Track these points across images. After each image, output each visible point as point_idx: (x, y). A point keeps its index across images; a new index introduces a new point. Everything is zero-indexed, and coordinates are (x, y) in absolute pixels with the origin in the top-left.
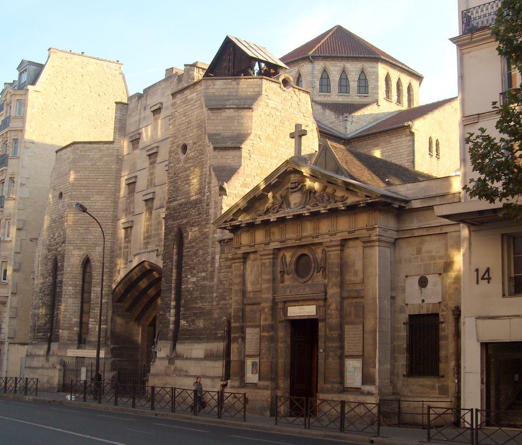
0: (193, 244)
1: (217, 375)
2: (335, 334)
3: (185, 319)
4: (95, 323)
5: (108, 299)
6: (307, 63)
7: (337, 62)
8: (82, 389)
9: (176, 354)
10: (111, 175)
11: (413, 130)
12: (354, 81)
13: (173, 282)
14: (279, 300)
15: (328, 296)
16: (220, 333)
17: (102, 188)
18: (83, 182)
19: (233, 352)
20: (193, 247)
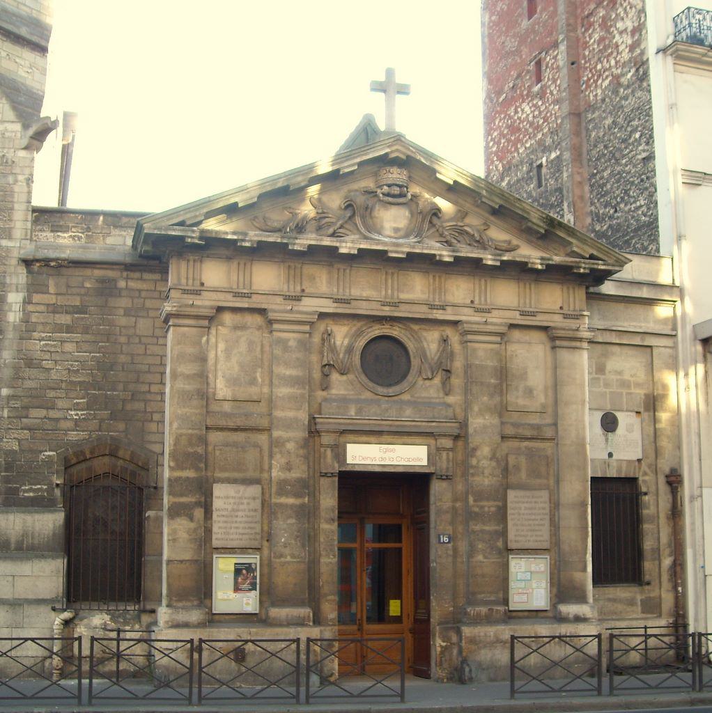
1: (31, 596)
2: (490, 506)
14: (327, 427)
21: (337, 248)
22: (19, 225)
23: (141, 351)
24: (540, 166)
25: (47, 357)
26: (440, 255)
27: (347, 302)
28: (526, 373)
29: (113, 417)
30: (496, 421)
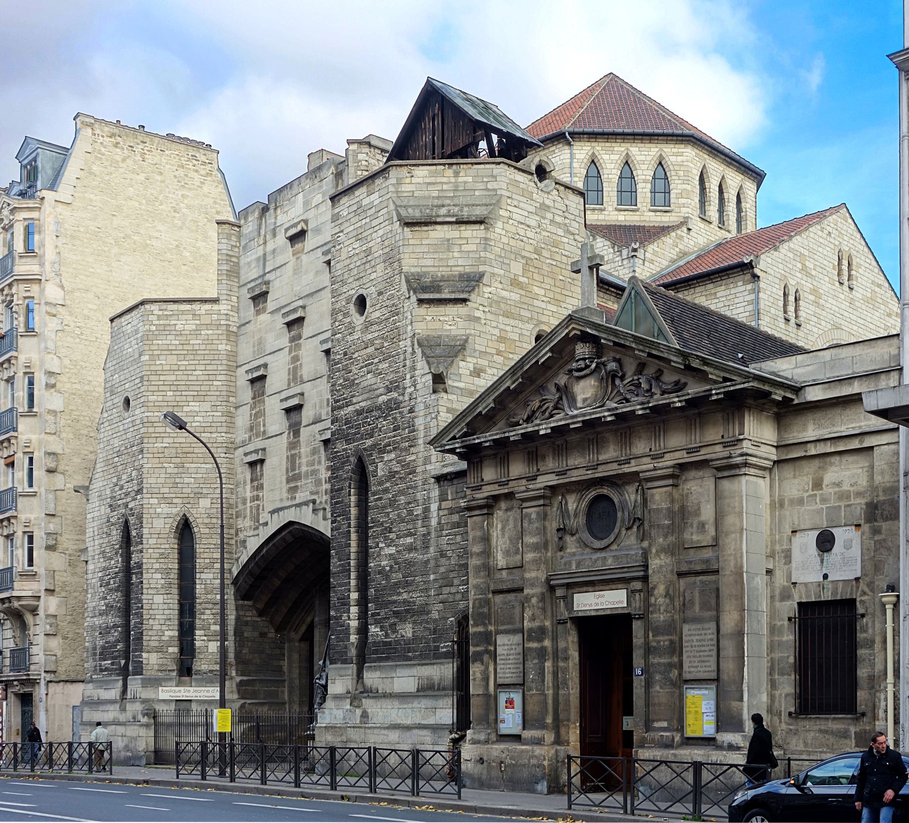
0: (388, 485)
3: (376, 623)
4: (205, 638)
6: (561, 145)
7: (614, 144)
8: (197, 757)
9: (364, 686)
10: (219, 362)
11: (757, 271)
12: (645, 181)
13: (353, 556)
15: (650, 572)
16: (445, 647)
17: (203, 388)
18: (168, 378)
19: (474, 679)
20: (386, 491)
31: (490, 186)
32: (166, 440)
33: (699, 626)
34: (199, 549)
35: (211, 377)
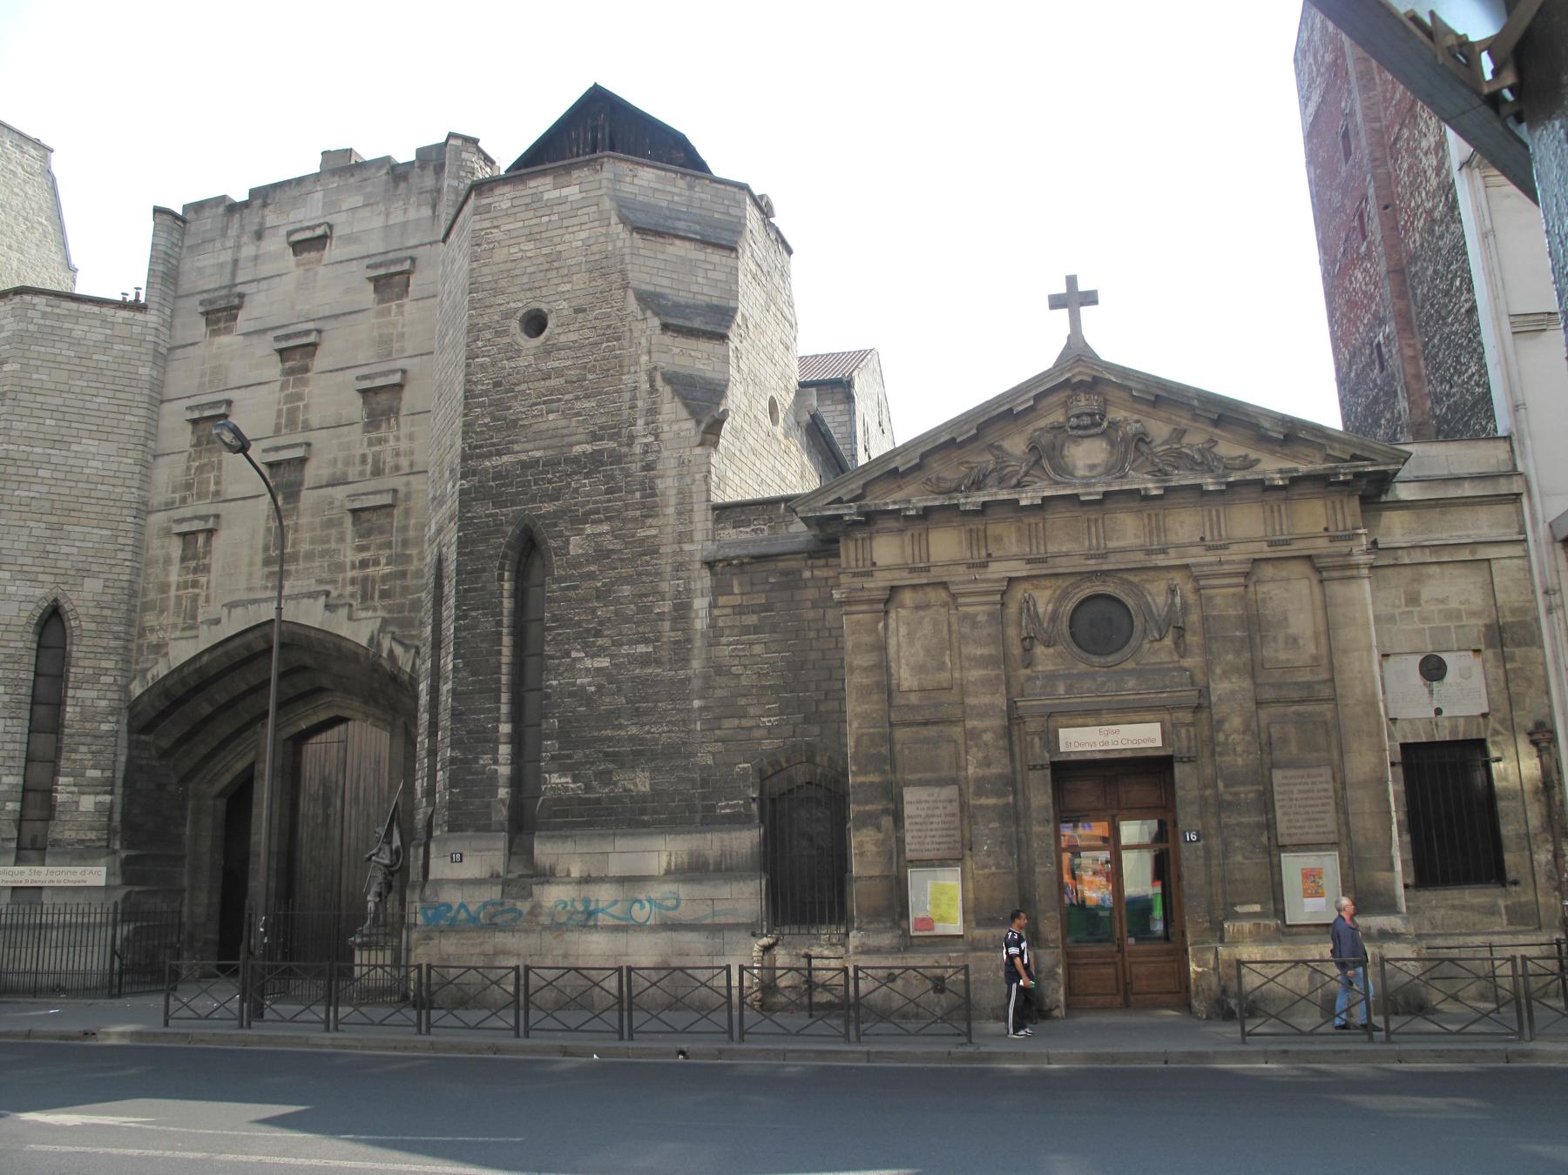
0: (593, 568)
2: (1247, 792)
4: (76, 789)
5: (117, 722)
13: (505, 669)
17: (107, 422)
18: (50, 400)
20: (591, 576)
21: (1017, 501)
22: (699, 526)
23: (832, 645)
24: (1379, 345)
25: (736, 662)
26: (1146, 489)
27: (1043, 561)
28: (1286, 619)
29: (806, 720)
30: (1247, 684)
31: (732, 211)
32: (35, 487)
33: (1301, 772)
34: (76, 651)
35: (122, 409)
